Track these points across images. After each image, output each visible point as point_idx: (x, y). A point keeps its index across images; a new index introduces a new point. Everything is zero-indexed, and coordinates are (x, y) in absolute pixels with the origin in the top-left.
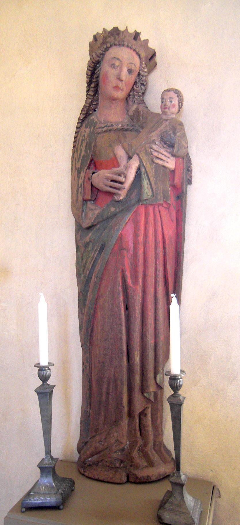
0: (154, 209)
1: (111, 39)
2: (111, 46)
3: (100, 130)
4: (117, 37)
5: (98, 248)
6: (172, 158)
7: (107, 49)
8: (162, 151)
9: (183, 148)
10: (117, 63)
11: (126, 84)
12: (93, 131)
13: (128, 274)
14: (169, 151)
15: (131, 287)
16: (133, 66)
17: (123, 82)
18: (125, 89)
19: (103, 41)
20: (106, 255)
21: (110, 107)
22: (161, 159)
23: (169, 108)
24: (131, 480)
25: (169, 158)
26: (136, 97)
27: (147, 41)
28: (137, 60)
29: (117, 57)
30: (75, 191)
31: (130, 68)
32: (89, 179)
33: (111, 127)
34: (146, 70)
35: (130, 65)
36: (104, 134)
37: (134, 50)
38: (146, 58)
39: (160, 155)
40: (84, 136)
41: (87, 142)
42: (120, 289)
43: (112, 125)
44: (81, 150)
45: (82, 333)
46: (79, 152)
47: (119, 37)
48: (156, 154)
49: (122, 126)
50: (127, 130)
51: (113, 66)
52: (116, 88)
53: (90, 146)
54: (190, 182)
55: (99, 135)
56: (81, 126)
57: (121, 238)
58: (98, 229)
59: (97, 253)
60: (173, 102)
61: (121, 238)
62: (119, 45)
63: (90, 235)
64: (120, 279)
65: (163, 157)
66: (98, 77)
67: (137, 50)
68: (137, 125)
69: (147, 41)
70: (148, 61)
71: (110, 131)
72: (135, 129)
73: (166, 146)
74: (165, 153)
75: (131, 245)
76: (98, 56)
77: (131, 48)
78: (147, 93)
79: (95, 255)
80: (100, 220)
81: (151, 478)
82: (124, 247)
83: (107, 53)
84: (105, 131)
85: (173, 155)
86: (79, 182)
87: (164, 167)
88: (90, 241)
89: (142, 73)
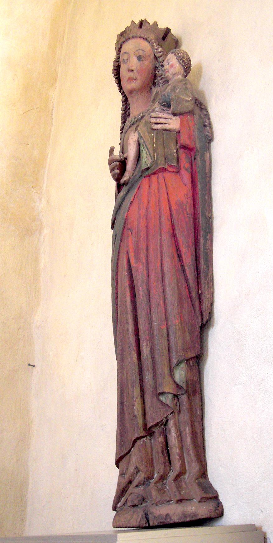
6: (174, 118)
9: (184, 102)
11: (138, 72)
13: (132, 255)
16: (141, 52)
17: (135, 72)
18: (139, 78)
24: (151, 524)
25: (171, 119)
27: (155, 24)
28: (146, 46)
34: (160, 49)
35: (137, 52)
37: (140, 37)
38: (157, 39)
39: (158, 119)
45: (119, 359)
48: (153, 120)
54: (209, 140)
60: (171, 63)
65: (162, 121)
67: (142, 35)
69: (155, 24)
70: (161, 40)
73: (165, 108)
77: (136, 37)
81: (170, 518)
85: (174, 114)
87: (166, 130)
89: (157, 55)
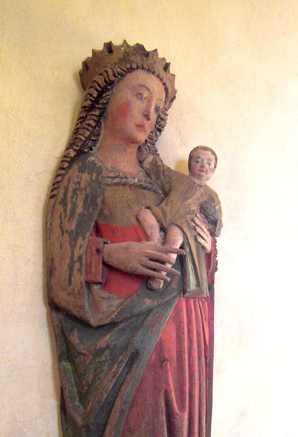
0: (195, 302)
1: (137, 59)
2: (138, 68)
3: (109, 181)
4: (145, 59)
5: (125, 358)
7: (131, 70)
8: (203, 227)
10: (146, 94)
12: (97, 179)
13: (173, 396)
14: (207, 227)
15: (177, 414)
19: (124, 57)
20: (141, 368)
21: (125, 150)
22: (203, 238)
23: (206, 172)
26: (149, 144)
29: (147, 86)
30: (66, 267)
31: (158, 105)
32: (98, 251)
33: (125, 180)
36: (116, 188)
40: (79, 183)
41: (87, 197)
42: (164, 418)
43: (126, 177)
44: (75, 205)
46: (69, 206)
47: (147, 60)
49: (138, 181)
50: (144, 188)
51: (139, 96)
52: (141, 127)
53: (95, 204)
55: (108, 188)
56: (69, 167)
57: (160, 344)
58: (123, 329)
59: (123, 365)
61: (160, 344)
62: (148, 70)
63: (108, 337)
64: (163, 404)
65: (205, 237)
66: (107, 103)
68: (155, 184)
71: (124, 184)
72: (154, 188)
74: (205, 230)
75: (174, 355)
76: (114, 75)
78: (75, 124)
79: (121, 370)
80: (128, 315)
82: (167, 357)
83: (129, 76)
84: (117, 184)
86: (73, 254)
88: (108, 347)
